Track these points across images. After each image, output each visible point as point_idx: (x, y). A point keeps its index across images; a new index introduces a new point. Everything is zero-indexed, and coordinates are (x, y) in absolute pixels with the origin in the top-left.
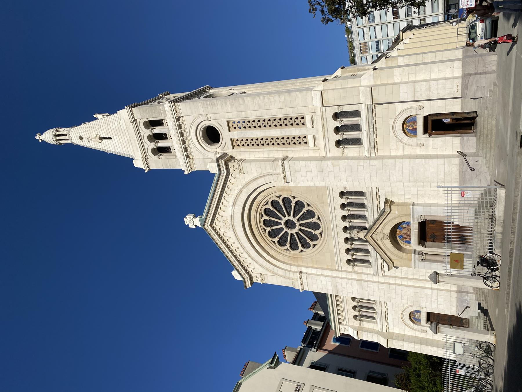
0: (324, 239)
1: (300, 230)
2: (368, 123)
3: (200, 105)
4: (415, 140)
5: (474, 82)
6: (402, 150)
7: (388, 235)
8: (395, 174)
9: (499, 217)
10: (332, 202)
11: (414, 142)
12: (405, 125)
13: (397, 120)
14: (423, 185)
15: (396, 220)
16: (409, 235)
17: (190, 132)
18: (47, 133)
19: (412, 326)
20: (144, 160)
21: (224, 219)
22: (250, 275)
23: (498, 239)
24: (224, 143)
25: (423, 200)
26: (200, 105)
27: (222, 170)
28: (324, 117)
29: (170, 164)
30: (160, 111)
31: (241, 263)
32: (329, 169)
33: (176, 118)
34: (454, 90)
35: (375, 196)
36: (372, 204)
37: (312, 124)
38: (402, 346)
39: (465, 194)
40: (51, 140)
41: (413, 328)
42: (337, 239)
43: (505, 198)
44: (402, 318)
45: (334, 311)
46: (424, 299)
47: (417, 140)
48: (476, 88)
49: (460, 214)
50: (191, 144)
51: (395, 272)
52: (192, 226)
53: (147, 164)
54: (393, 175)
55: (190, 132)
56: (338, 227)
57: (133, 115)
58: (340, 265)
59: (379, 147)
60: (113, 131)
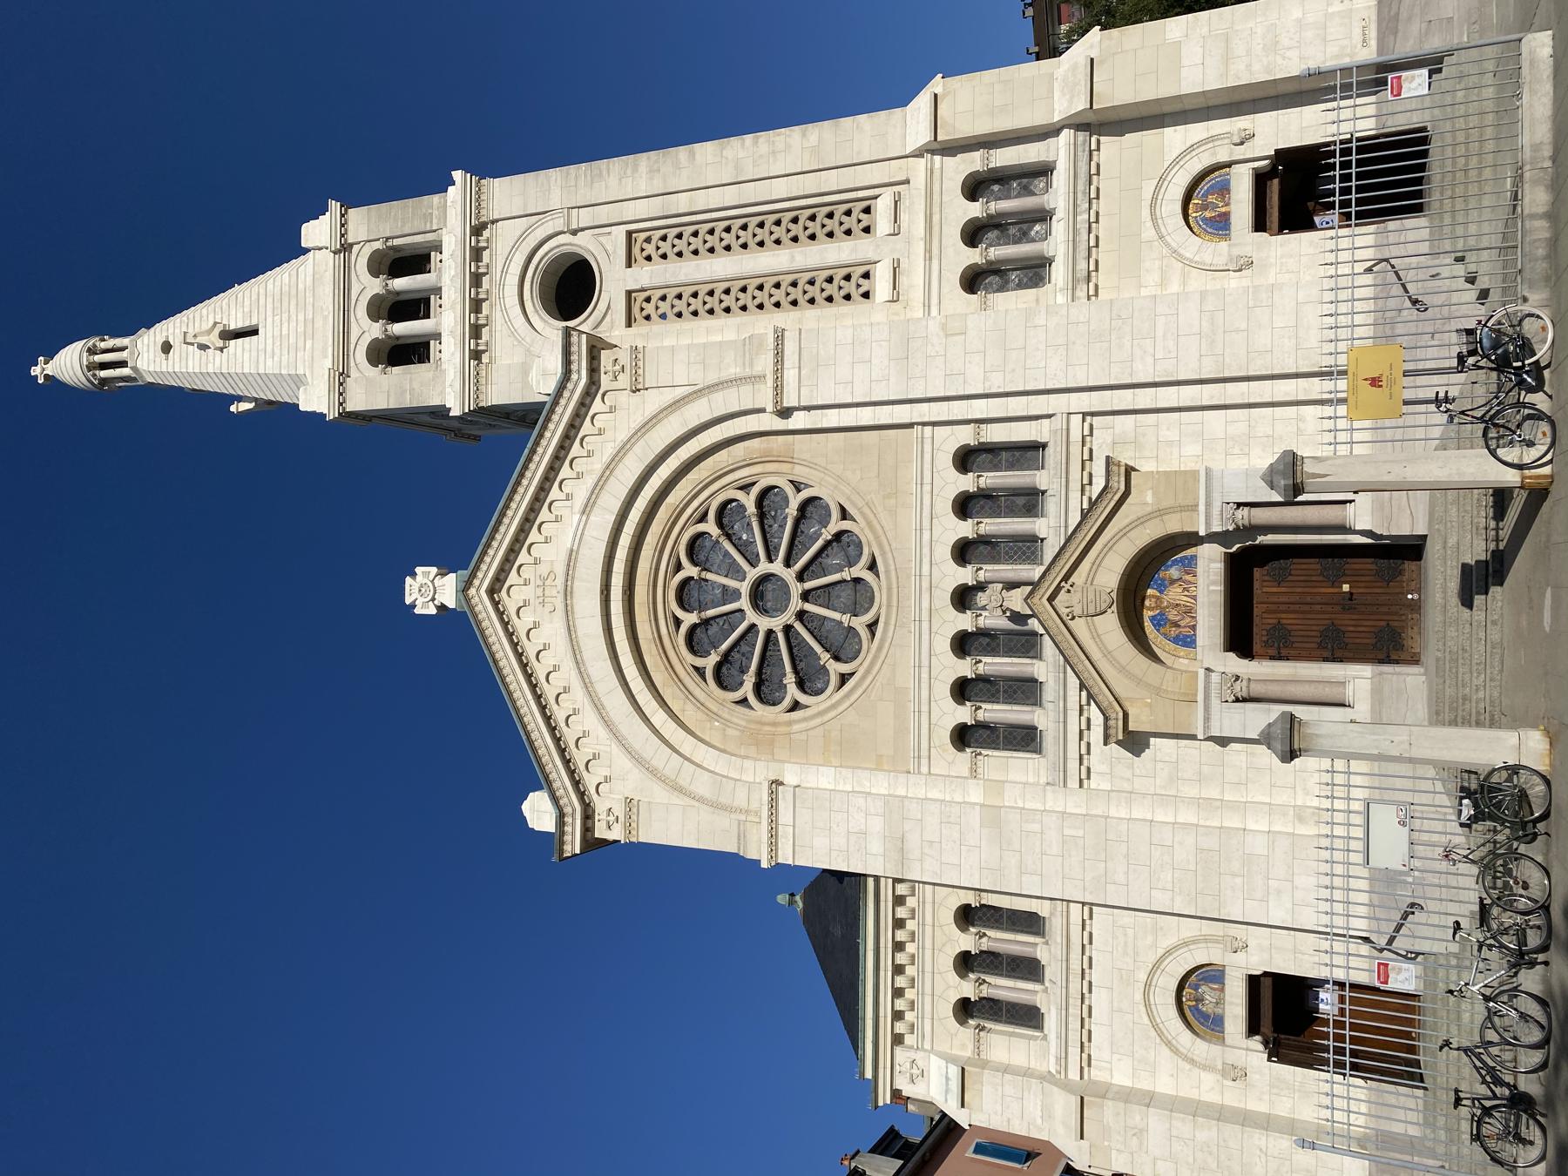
0: (880, 648)
1: (801, 615)
2: (1071, 194)
3: (556, 180)
4: (1215, 1049)
5: (1417, 10)
6: (1180, 285)
7: (1114, 595)
8: (1152, 351)
9: (1536, 148)
10: (927, 488)
11: (1220, 255)
12: (1191, 206)
13: (1166, 183)
14: (1246, 391)
15: (1145, 529)
16: (1189, 611)
17: (503, 272)
18: (64, 354)
19: (1188, 1045)
20: (334, 378)
21: (543, 569)
22: (589, 805)
23: (1537, 244)
24: (602, 306)
25: (1245, 461)
26: (556, 180)
27: (574, 367)
28: (936, 188)
29: (412, 390)
30: (430, 211)
31: (564, 750)
32: (929, 346)
33: (473, 224)
34: (1354, 41)
35: (1075, 449)
36: (1064, 480)
37: (892, 288)
38: (1141, 1131)
39: (1405, 85)
40: (74, 365)
41: (1190, 1055)
42: (925, 637)
43: (1552, 63)
44: (1147, 1005)
45: (882, 973)
46: (1239, 880)
47: (1229, 245)
48: (1424, 25)
49: (1376, 782)
50: (498, 317)
51: (1128, 774)
52: (426, 609)
53: (341, 394)
54: (1145, 352)
55: (503, 272)
56: (936, 587)
57: (344, 388)
58: (924, 753)
59: (1102, 278)
60: (270, 300)
